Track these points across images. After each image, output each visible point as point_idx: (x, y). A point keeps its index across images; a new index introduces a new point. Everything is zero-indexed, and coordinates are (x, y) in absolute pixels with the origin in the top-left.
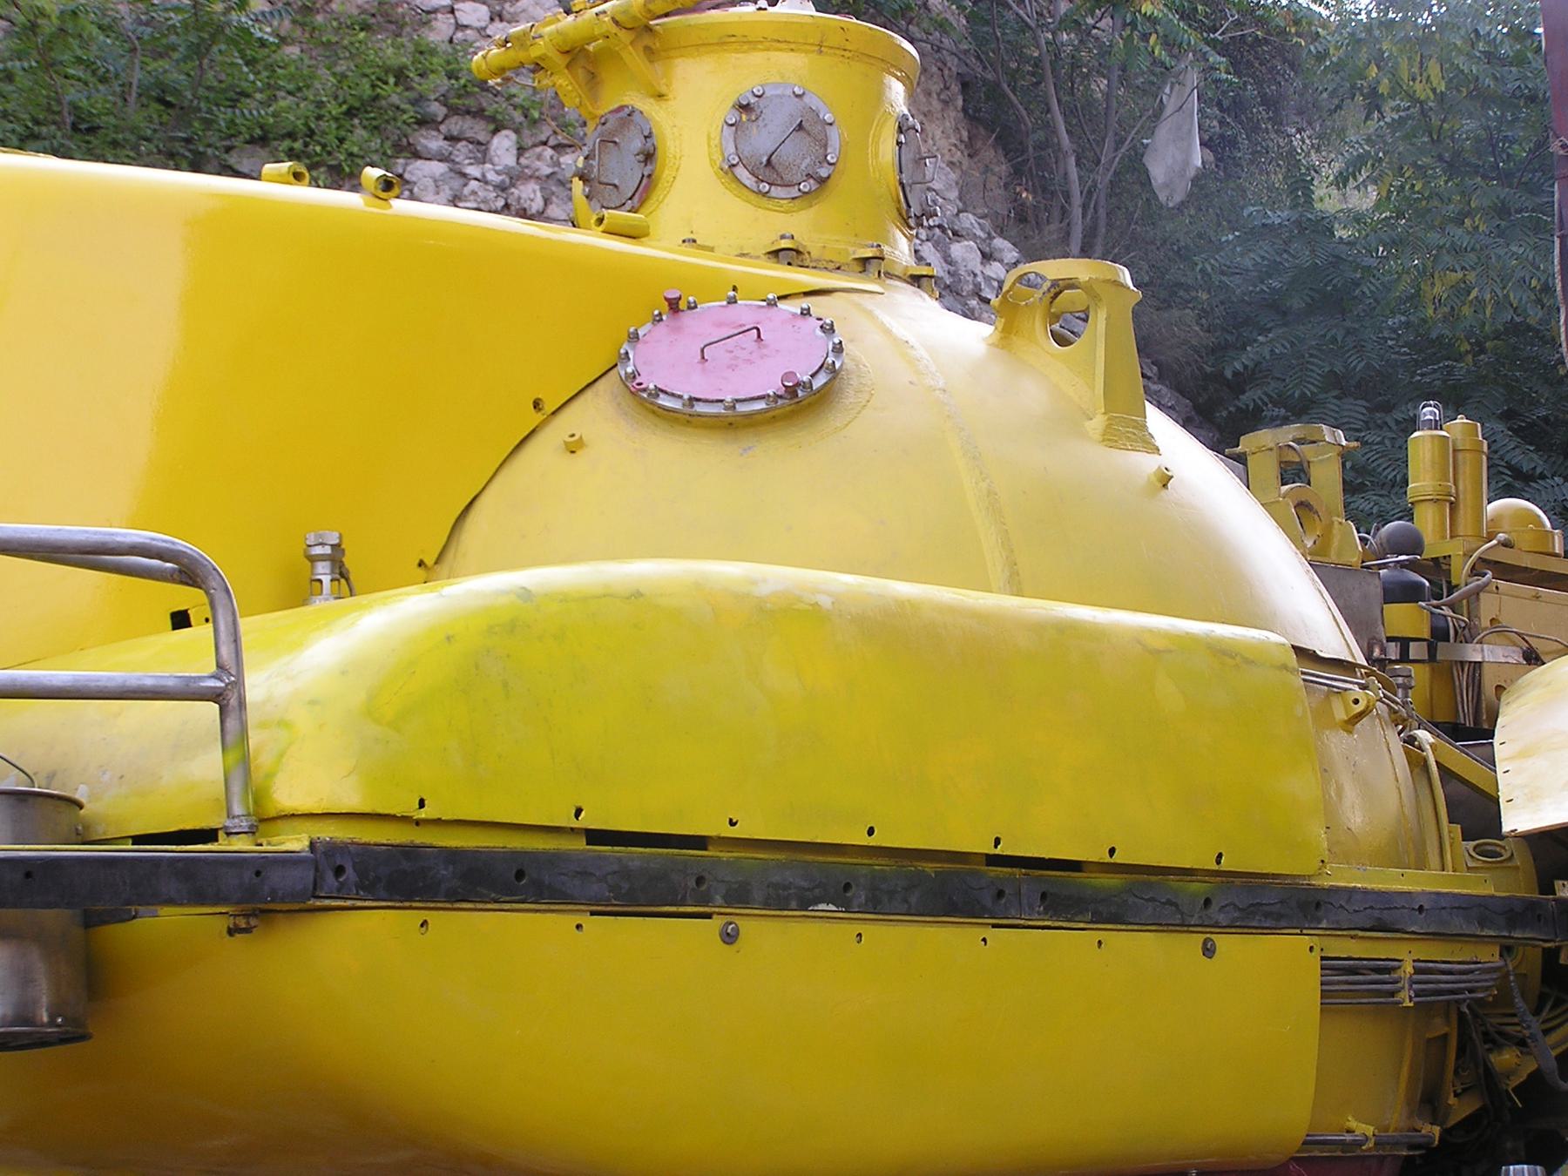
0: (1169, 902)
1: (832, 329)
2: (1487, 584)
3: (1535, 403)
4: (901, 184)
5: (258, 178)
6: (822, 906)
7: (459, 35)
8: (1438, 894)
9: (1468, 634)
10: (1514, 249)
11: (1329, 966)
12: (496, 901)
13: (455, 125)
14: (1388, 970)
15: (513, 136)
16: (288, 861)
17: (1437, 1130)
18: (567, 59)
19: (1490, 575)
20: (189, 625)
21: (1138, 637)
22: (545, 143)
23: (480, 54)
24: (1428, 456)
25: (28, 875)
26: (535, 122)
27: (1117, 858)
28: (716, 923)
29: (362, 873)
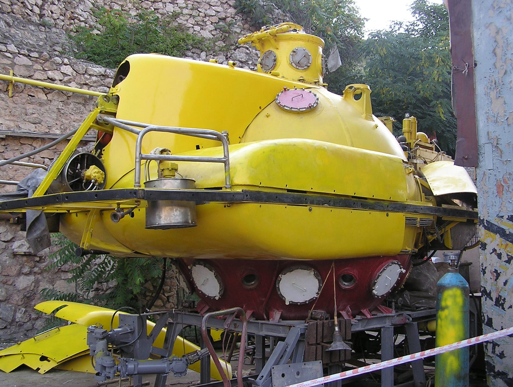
0: (382, 206)
1: (316, 96)
2: (418, 148)
3: (399, 114)
4: (322, 68)
5: (209, 61)
6: (326, 205)
7: (194, 32)
8: (425, 206)
9: (415, 157)
10: (399, 84)
11: (407, 219)
12: (273, 202)
13: (194, 50)
14: (415, 220)
15: (205, 53)
16: (238, 193)
17: (417, 250)
18: (259, 41)
19: (419, 146)
20: (199, 149)
21: (377, 156)
22: (211, 54)
23: (241, 39)
24: (407, 123)
25: (193, 195)
26: (209, 50)
27: (374, 198)
28: (308, 207)
29: (251, 196)
